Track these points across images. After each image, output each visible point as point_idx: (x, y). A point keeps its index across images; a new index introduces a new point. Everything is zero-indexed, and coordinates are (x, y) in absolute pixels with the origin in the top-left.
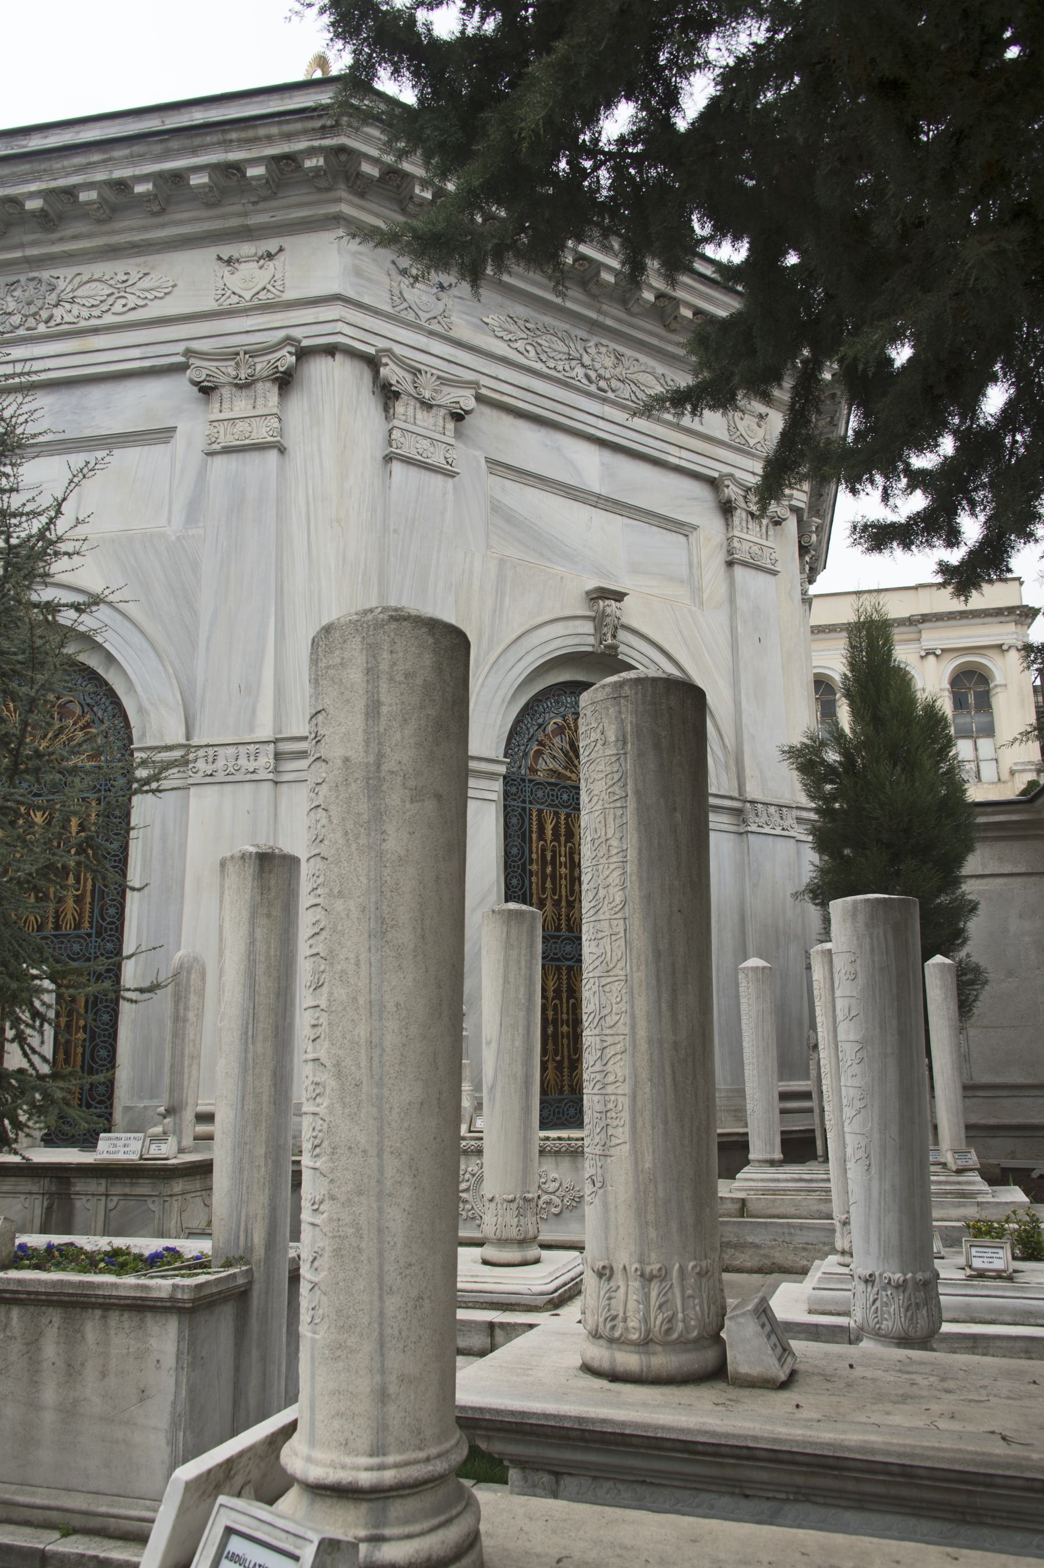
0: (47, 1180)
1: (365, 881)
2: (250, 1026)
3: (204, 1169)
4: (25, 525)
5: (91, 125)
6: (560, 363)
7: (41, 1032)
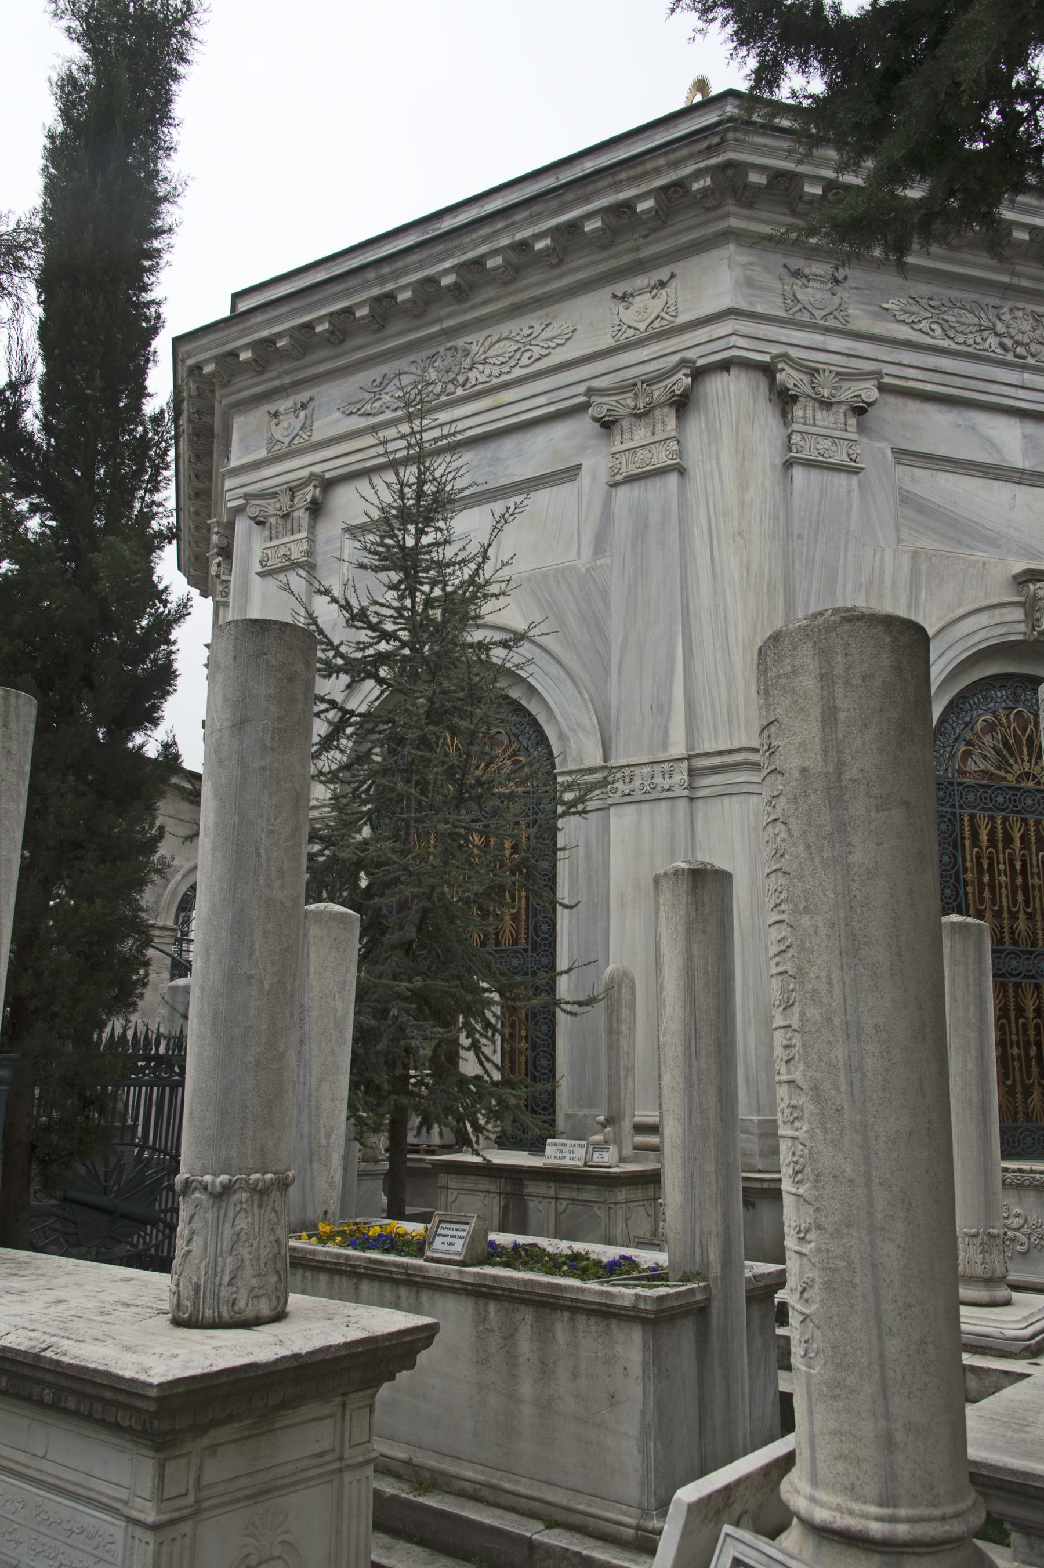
0: (503, 1180)
1: (832, 896)
2: (693, 1042)
3: (653, 1179)
4: (458, 573)
5: (495, 196)
6: (970, 336)
7: (494, 1042)
